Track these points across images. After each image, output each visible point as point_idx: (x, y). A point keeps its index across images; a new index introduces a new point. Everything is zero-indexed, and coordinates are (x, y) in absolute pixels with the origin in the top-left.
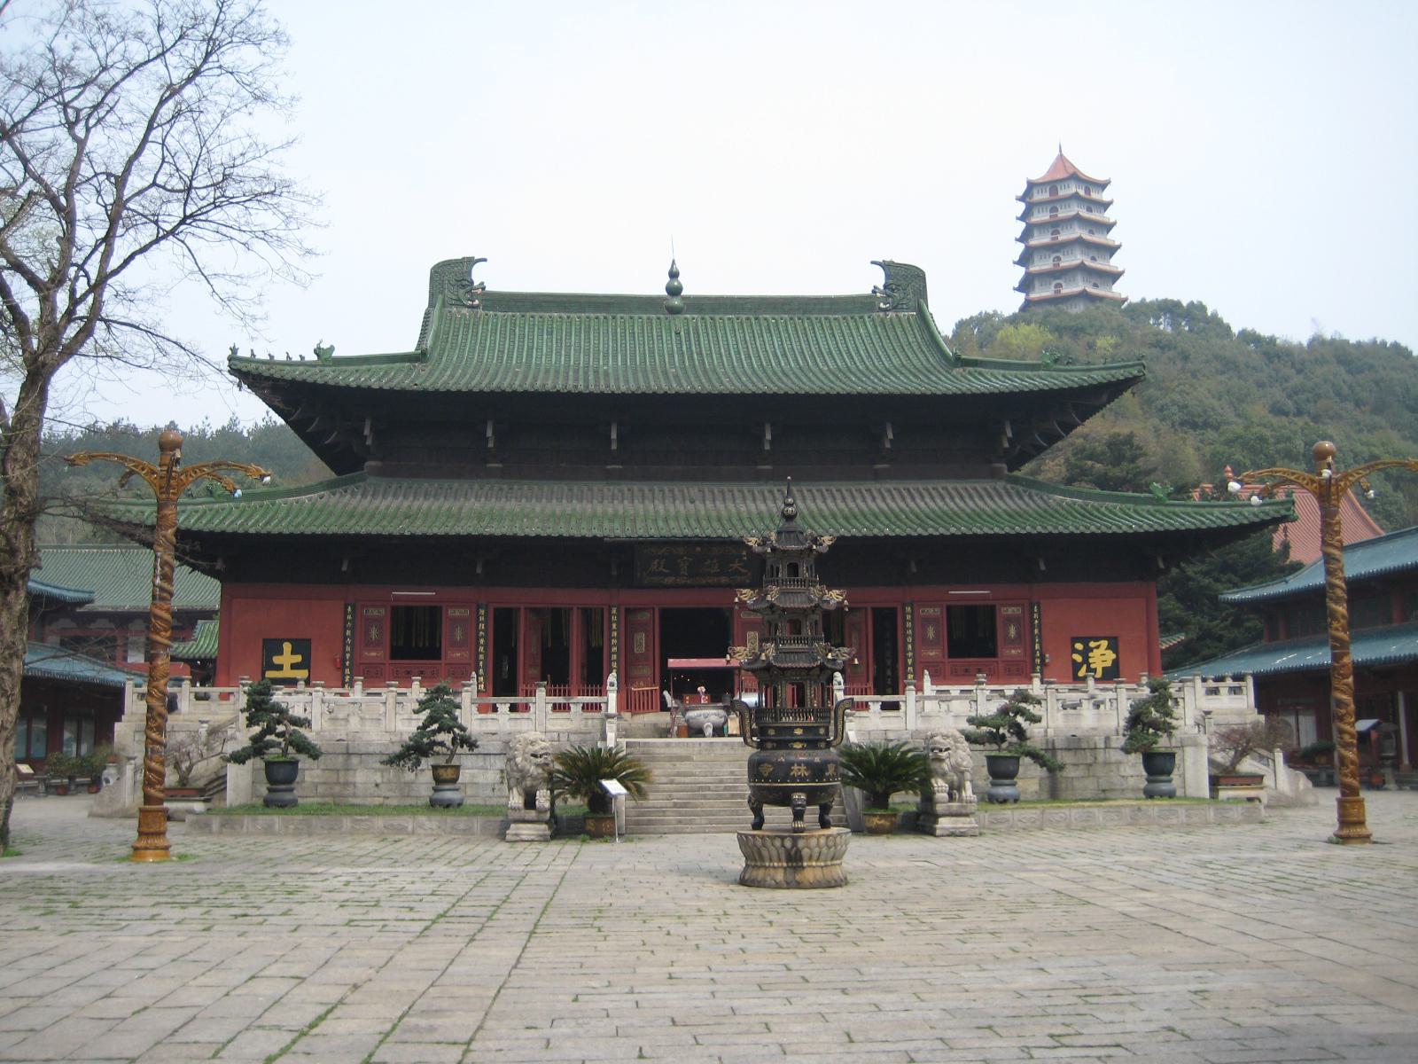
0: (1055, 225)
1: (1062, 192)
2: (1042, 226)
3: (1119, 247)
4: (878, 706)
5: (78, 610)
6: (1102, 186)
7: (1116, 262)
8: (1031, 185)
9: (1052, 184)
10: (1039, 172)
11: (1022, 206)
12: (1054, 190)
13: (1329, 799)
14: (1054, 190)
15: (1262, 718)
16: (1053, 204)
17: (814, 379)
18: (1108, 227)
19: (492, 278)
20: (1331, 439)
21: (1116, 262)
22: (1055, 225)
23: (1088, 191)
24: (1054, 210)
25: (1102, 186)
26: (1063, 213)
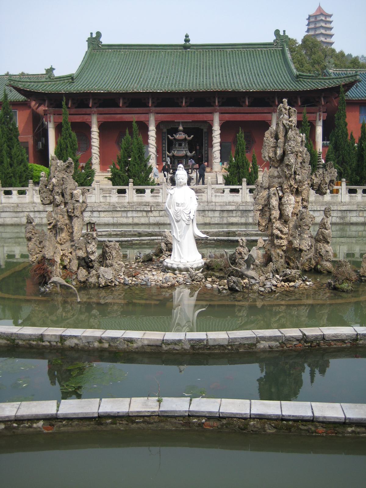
0: (315, 29)
1: (318, 19)
2: (312, 29)
3: (333, 28)
4: (115, 191)
5: (127, 131)
6: (330, 16)
7: (332, 32)
8: (310, 16)
9: (315, 16)
10: (312, 12)
11: (307, 22)
12: (316, 18)
13: (286, 34)
14: (316, 18)
15: (300, 43)
16: (315, 22)
17: (285, 85)
18: (331, 29)
19: (105, 40)
20: (55, 372)
21: (332, 32)
22: (315, 29)
23: (326, 18)
24: (316, 24)
25: (330, 16)
26: (318, 25)
